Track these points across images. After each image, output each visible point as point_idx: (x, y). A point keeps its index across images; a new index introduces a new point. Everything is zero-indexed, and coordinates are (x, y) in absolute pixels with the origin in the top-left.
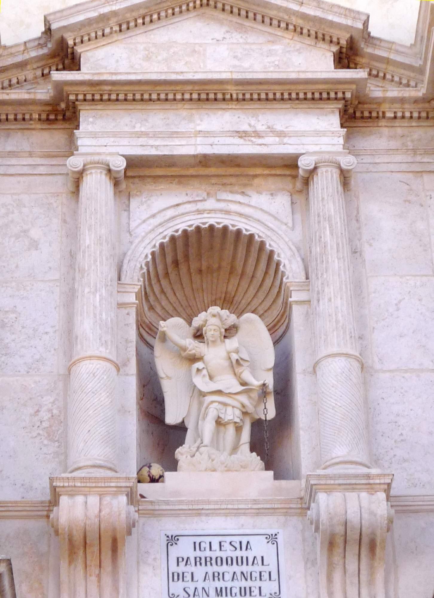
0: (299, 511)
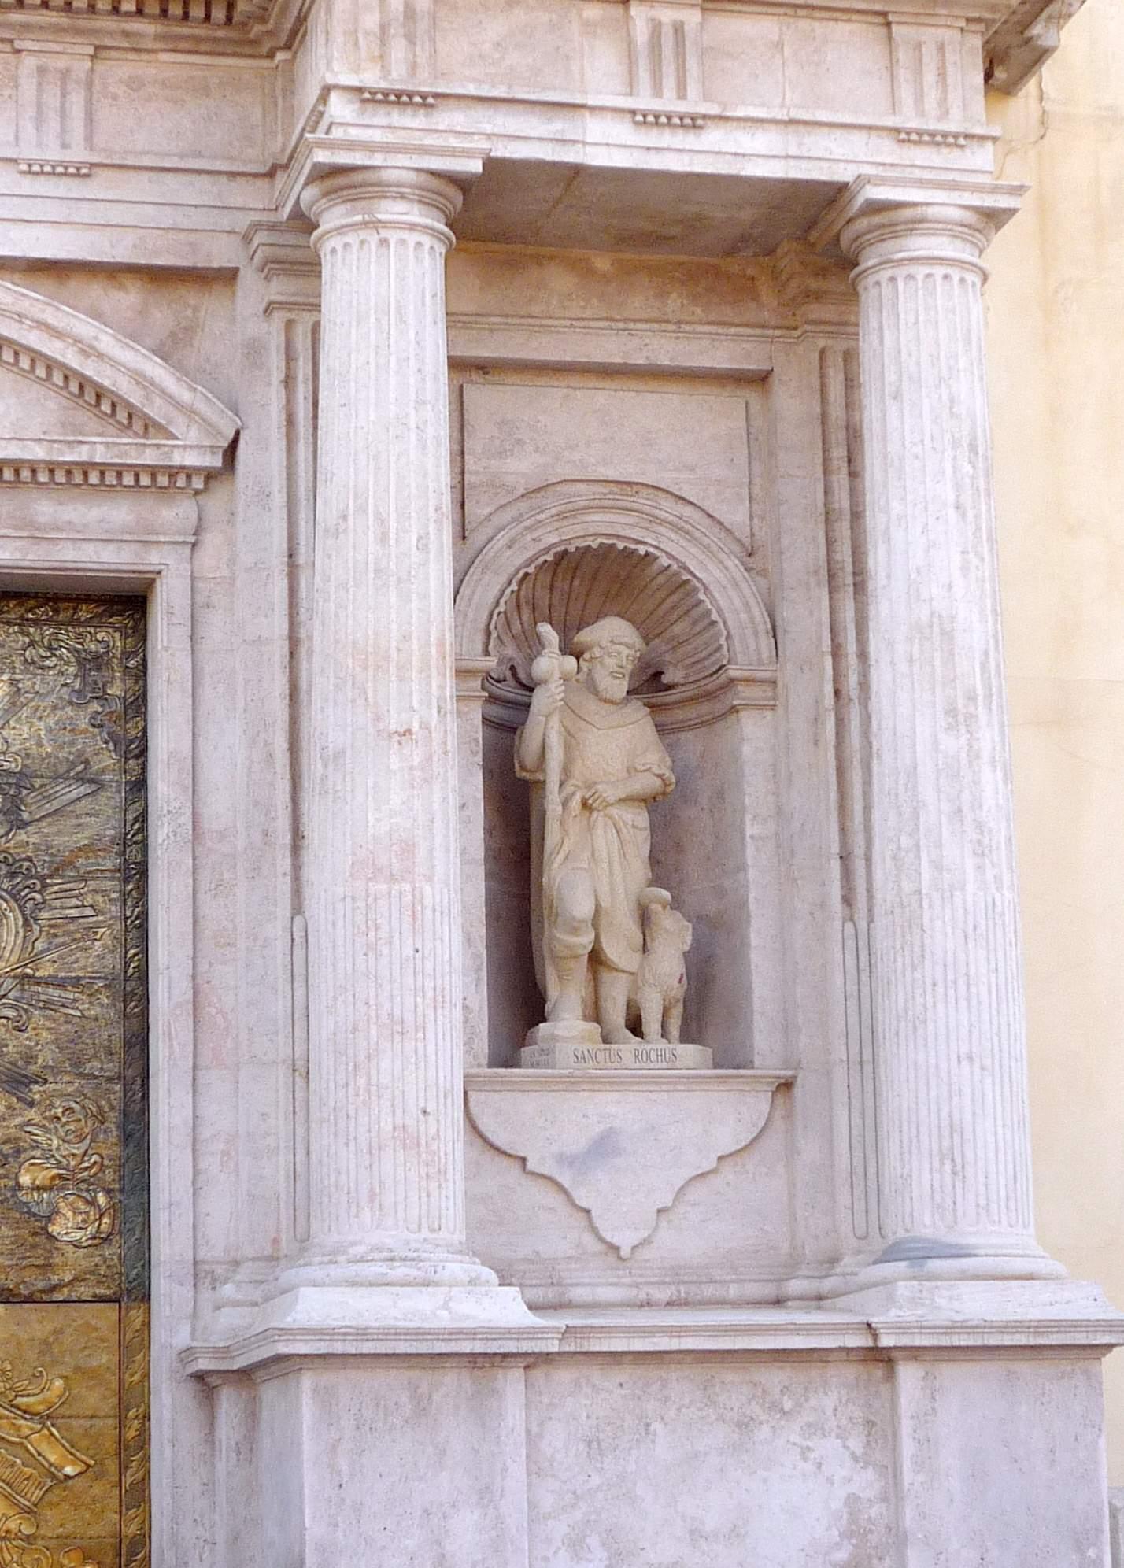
0: (982, 1252)
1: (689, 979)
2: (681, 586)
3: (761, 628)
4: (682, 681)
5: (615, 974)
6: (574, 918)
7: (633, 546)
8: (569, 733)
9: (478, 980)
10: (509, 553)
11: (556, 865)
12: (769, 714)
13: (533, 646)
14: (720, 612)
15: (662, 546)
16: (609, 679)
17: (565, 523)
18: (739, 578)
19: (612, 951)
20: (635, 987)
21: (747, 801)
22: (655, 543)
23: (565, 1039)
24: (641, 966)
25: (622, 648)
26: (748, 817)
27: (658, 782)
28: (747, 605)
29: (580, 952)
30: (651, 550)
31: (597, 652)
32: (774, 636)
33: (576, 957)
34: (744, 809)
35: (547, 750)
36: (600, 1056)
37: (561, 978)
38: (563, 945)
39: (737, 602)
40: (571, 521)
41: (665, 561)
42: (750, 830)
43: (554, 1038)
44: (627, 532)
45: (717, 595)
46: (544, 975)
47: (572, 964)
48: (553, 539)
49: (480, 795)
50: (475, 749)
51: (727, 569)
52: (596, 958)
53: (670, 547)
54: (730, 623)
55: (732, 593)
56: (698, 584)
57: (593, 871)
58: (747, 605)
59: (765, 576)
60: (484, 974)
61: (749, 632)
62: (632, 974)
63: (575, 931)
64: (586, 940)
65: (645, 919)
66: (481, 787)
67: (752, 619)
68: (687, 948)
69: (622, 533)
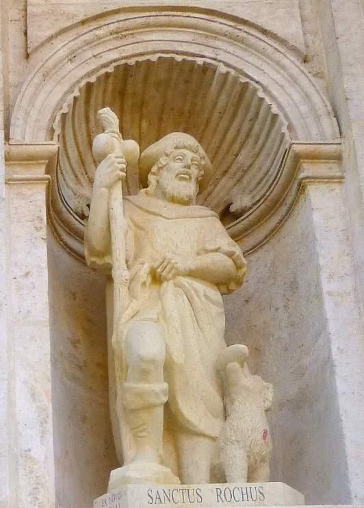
1: (272, 434)
2: (243, 94)
3: (322, 110)
4: (249, 204)
5: (196, 439)
6: (142, 359)
7: (190, 58)
8: (138, 226)
9: (44, 432)
10: (70, 66)
11: (123, 321)
12: (336, 187)
13: (93, 127)
14: (280, 106)
15: (219, 58)
16: (177, 182)
17: (124, 42)
18: (295, 71)
19: (193, 412)
20: (219, 451)
21: (322, 261)
22: (212, 56)
23: (138, 481)
24: (224, 429)
25: (186, 152)
26: (324, 277)
27: (229, 262)
28: (307, 96)
29: (153, 400)
30: (209, 61)
31: (163, 161)
32: (336, 116)
33: (149, 407)
34: (318, 269)
35: (112, 221)
36: (178, 496)
37: (135, 436)
38: (138, 390)
39: (297, 97)
40: (131, 40)
41: (223, 69)
42: (326, 287)
43: (125, 480)
44: (185, 48)
45: (275, 93)
46: (119, 429)
47: (144, 416)
48: (114, 55)
49: (45, 265)
50: (38, 225)
51: (283, 67)
52: (174, 425)
53: (225, 55)
54: (291, 115)
55: (290, 90)
56: (257, 86)
57: (163, 329)
58: (307, 96)
59: (322, 77)
60: (50, 427)
61: (310, 120)
62: (214, 439)
63: (144, 374)
64: (157, 387)
65: (224, 384)
66: (46, 258)
67: (313, 108)
68: (268, 404)
69: (180, 49)
